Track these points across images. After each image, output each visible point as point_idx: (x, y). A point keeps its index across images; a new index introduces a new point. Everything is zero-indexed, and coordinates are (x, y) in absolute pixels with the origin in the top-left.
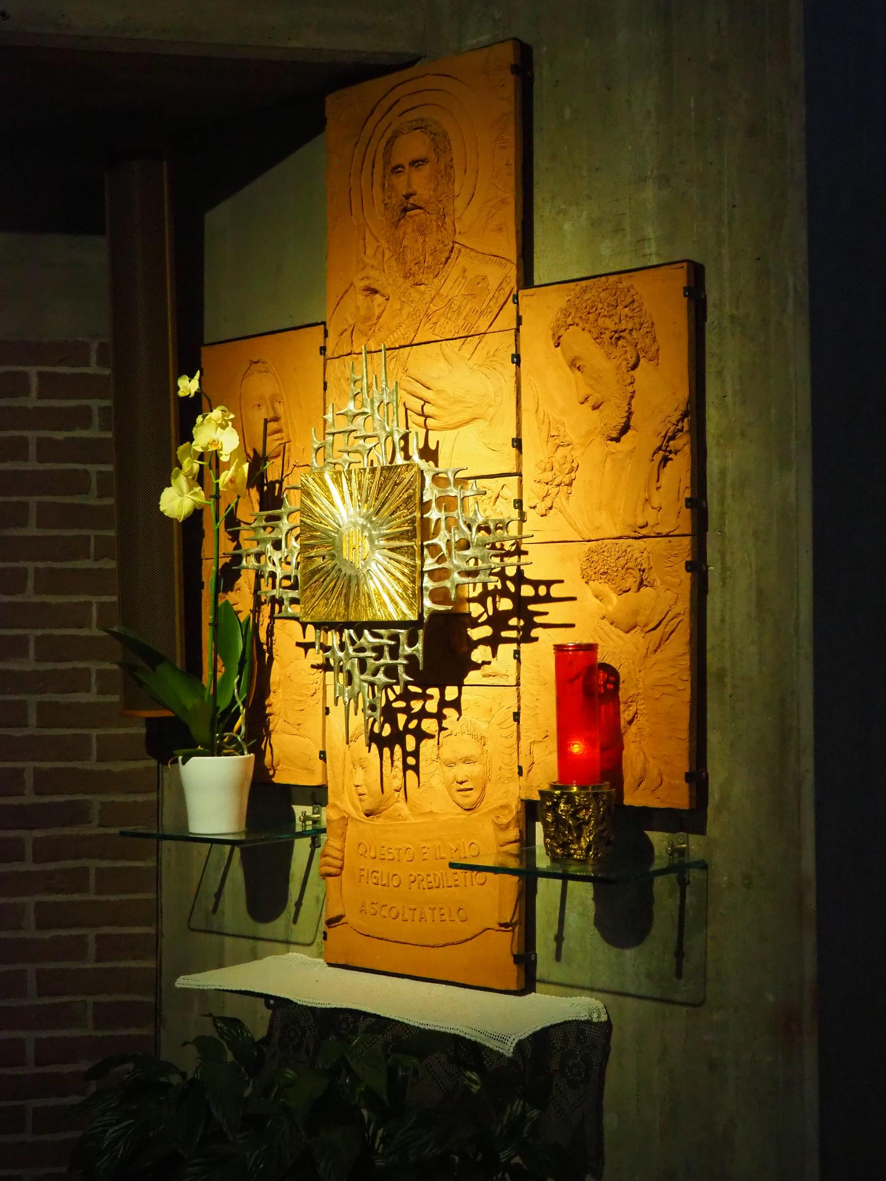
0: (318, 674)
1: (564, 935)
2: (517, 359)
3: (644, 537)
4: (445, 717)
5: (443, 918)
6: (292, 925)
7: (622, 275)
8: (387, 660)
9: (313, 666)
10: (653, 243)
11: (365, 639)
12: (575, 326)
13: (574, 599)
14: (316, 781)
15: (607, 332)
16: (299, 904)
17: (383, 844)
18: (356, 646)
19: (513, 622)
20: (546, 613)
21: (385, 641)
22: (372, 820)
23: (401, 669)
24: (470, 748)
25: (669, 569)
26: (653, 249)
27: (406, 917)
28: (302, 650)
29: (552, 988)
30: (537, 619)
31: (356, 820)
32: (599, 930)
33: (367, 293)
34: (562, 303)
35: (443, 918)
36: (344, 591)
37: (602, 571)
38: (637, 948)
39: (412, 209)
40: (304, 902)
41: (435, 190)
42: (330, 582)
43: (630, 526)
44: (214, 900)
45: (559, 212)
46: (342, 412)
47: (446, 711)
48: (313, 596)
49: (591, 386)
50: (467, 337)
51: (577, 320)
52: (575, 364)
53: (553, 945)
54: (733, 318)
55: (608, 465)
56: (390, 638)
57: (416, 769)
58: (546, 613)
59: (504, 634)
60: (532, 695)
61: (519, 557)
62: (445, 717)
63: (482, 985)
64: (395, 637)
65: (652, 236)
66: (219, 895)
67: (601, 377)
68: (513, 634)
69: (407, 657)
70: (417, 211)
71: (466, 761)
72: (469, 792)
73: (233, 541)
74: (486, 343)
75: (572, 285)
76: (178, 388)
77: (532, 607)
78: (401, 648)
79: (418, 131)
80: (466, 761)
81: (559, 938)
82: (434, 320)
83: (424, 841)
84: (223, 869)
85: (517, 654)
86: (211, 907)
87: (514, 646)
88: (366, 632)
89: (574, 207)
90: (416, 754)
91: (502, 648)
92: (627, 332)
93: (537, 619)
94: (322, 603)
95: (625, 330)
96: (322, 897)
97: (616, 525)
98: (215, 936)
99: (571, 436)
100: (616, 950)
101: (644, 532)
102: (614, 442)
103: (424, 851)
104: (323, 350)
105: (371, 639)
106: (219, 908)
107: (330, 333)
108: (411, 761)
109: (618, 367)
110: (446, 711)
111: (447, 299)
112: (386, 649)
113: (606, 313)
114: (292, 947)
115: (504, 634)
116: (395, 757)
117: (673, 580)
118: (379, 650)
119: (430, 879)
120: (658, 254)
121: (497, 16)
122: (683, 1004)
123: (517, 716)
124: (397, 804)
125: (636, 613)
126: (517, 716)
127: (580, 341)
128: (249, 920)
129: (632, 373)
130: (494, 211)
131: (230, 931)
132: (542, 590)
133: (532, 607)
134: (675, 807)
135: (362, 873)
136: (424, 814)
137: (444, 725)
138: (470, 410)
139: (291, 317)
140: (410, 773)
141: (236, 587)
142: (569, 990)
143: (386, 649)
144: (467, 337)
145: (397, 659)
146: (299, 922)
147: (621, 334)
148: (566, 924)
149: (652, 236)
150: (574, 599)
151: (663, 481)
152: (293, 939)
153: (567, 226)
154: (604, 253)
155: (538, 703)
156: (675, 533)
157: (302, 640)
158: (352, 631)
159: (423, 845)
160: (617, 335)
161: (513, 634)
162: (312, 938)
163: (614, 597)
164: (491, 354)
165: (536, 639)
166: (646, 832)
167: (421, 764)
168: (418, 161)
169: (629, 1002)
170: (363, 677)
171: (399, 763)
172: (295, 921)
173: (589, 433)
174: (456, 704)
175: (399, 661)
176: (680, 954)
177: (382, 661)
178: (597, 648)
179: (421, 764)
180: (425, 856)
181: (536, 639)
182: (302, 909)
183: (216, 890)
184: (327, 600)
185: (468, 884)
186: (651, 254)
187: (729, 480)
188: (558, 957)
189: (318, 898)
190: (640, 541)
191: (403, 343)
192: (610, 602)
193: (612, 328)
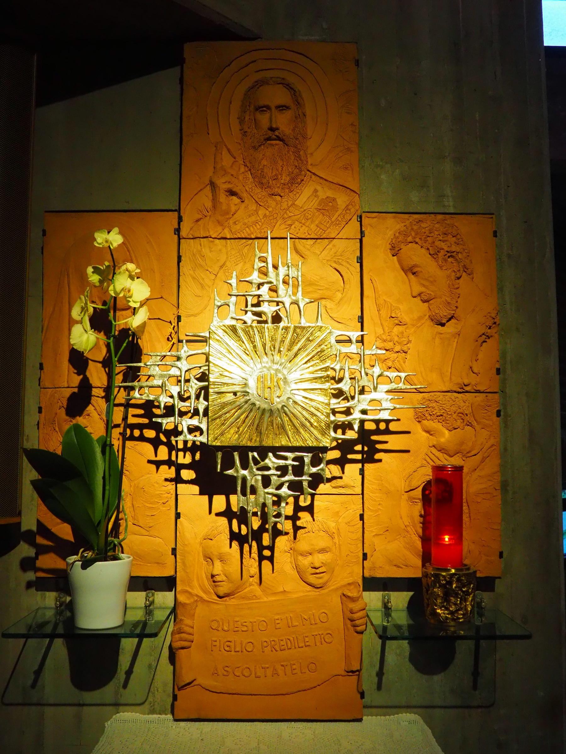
0: (171, 486)
1: (384, 671)
2: (360, 260)
3: (467, 392)
4: (299, 518)
5: (295, 672)
6: (121, 690)
7: (447, 216)
8: (290, 477)
9: (166, 480)
10: (451, 199)
11: (270, 459)
12: (414, 244)
13: (409, 432)
14: (169, 572)
15: (441, 251)
16: (129, 672)
17: (237, 619)
18: (258, 466)
19: (358, 448)
20: (386, 442)
21: (290, 462)
22: (226, 601)
23: (305, 484)
24: (323, 542)
25: (485, 415)
26: (451, 204)
27: (258, 674)
28: (154, 467)
29: (374, 710)
30: (378, 446)
31: (209, 602)
32: (412, 664)
33: (227, 194)
34: (399, 226)
35: (295, 672)
36: (256, 422)
37: (438, 414)
38: (442, 674)
39: (275, 140)
40: (135, 669)
41: (293, 130)
42: (242, 414)
43: (458, 384)
44: (33, 677)
45: (378, 166)
46: (247, 279)
47: (300, 514)
48: (223, 424)
49: (424, 286)
50: (317, 239)
51: (417, 240)
52: (411, 271)
53: (376, 680)
54: (509, 256)
55: (437, 341)
56: (294, 460)
57: (271, 559)
58: (386, 442)
59: (350, 456)
60: (375, 501)
61: (102, 398)
62: (299, 518)
63: (332, 719)
64: (300, 460)
65: (450, 194)
66: (38, 673)
67: (435, 281)
68: (359, 457)
69: (311, 475)
70: (278, 142)
71: (323, 551)
72: (322, 575)
73: (79, 374)
74: (334, 246)
75: (406, 216)
76: (120, 233)
77: (374, 438)
78: (306, 468)
79: (281, 85)
80: (323, 551)
81: (380, 674)
82: (289, 222)
83: (278, 614)
84: (44, 650)
85: (362, 472)
86: (30, 682)
87: (360, 466)
88: (270, 455)
89: (389, 165)
90: (271, 548)
91: (348, 467)
92: (455, 253)
93: (378, 446)
94: (232, 431)
95: (454, 252)
96: (154, 664)
97: (444, 382)
98: (33, 708)
99: (406, 318)
100: (425, 677)
101: (467, 389)
102: (440, 326)
103: (277, 622)
104: (178, 231)
105: (274, 460)
106: (40, 683)
107: (185, 218)
108: (267, 553)
109: (449, 277)
110: (300, 514)
111: (302, 210)
112: (290, 468)
113: (441, 239)
114: (121, 708)
115: (350, 456)
116: (253, 551)
117: (487, 422)
118: (283, 470)
119: (282, 643)
120: (455, 207)
121: (325, 26)
122: (479, 707)
123: (362, 517)
124: (251, 587)
125: (462, 443)
126: (362, 517)
127: (417, 254)
128: (76, 691)
129: (457, 281)
130: (341, 154)
131: (52, 701)
132: (382, 426)
133: (374, 438)
134: (491, 575)
135: (215, 643)
136: (275, 594)
137: (299, 523)
138: (321, 292)
139: (128, 202)
140: (266, 563)
141: (85, 413)
142: (388, 710)
143: (290, 468)
144: (317, 239)
145: (302, 476)
146: (130, 685)
147: (452, 254)
148: (386, 663)
149: (450, 194)
150: (409, 432)
151: (480, 356)
152: (122, 701)
153: (383, 177)
154: (413, 199)
155: (380, 507)
156: (488, 391)
157: (153, 458)
158: (255, 454)
159: (276, 617)
160: (449, 254)
161: (359, 457)
162: (145, 698)
163: (447, 432)
164: (338, 254)
165: (380, 461)
166: (73, 541)
167: (275, 555)
168: (282, 106)
169: (438, 711)
170: (266, 490)
171: (255, 555)
172: (125, 686)
173: (420, 318)
174: (310, 509)
175: (304, 478)
176: (476, 674)
177: (287, 478)
178: (463, 469)
179: (276, 555)
180: (278, 626)
181: (380, 461)
182: (132, 676)
183: (36, 667)
184: (238, 428)
185: (318, 644)
186: (449, 206)
187: (508, 359)
188: (379, 687)
189: (150, 666)
190: (461, 395)
191: (259, 236)
192: (443, 435)
193: (446, 248)
